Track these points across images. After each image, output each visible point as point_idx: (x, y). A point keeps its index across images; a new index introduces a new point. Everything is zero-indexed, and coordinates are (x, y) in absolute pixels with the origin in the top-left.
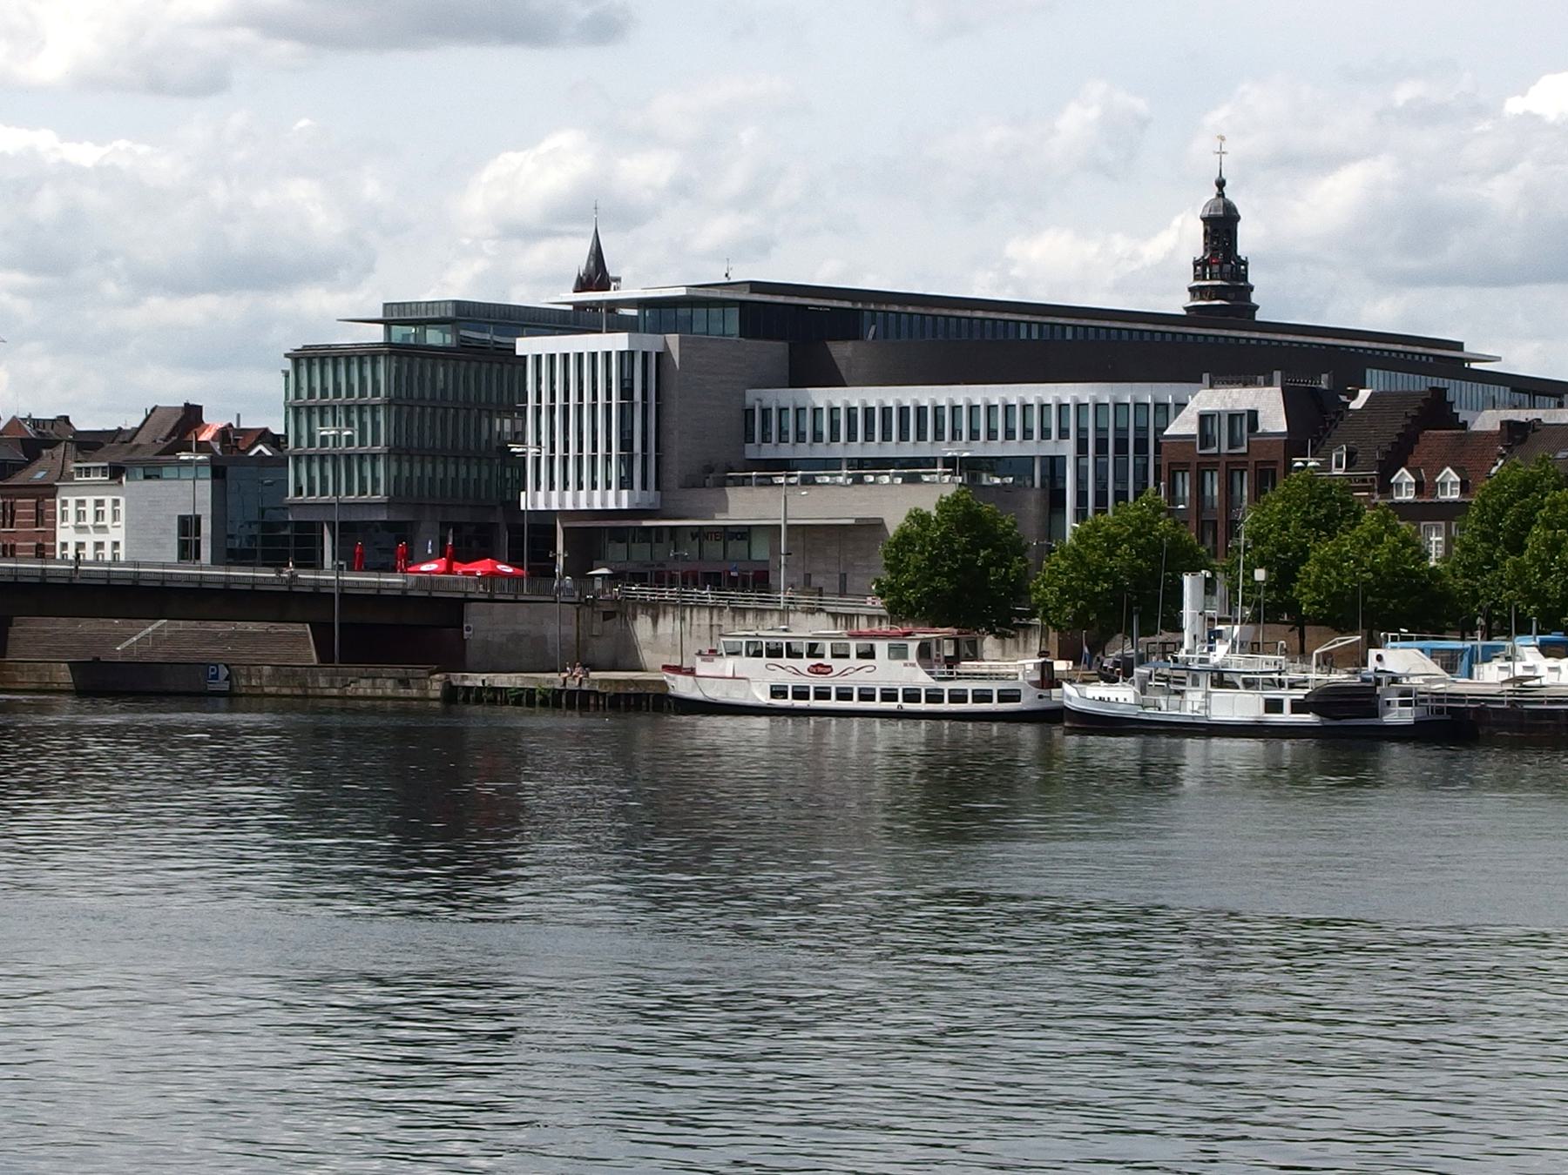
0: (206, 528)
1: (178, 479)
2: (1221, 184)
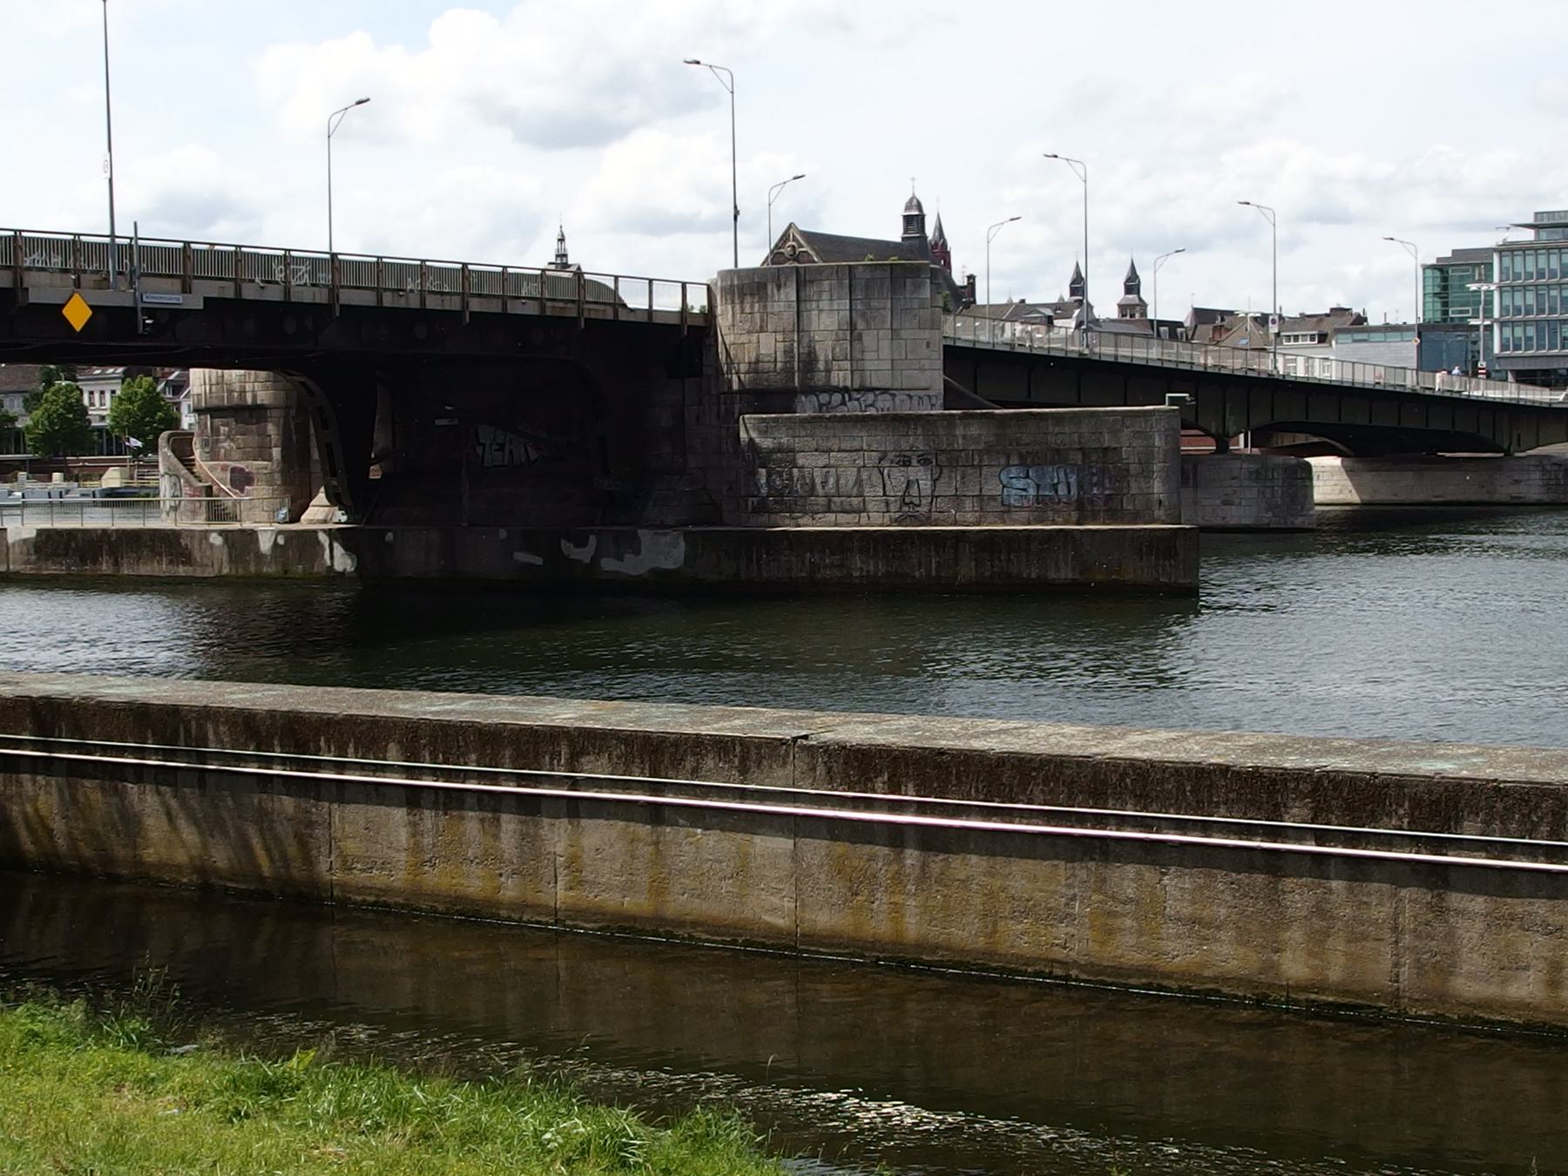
1: (1385, 341)
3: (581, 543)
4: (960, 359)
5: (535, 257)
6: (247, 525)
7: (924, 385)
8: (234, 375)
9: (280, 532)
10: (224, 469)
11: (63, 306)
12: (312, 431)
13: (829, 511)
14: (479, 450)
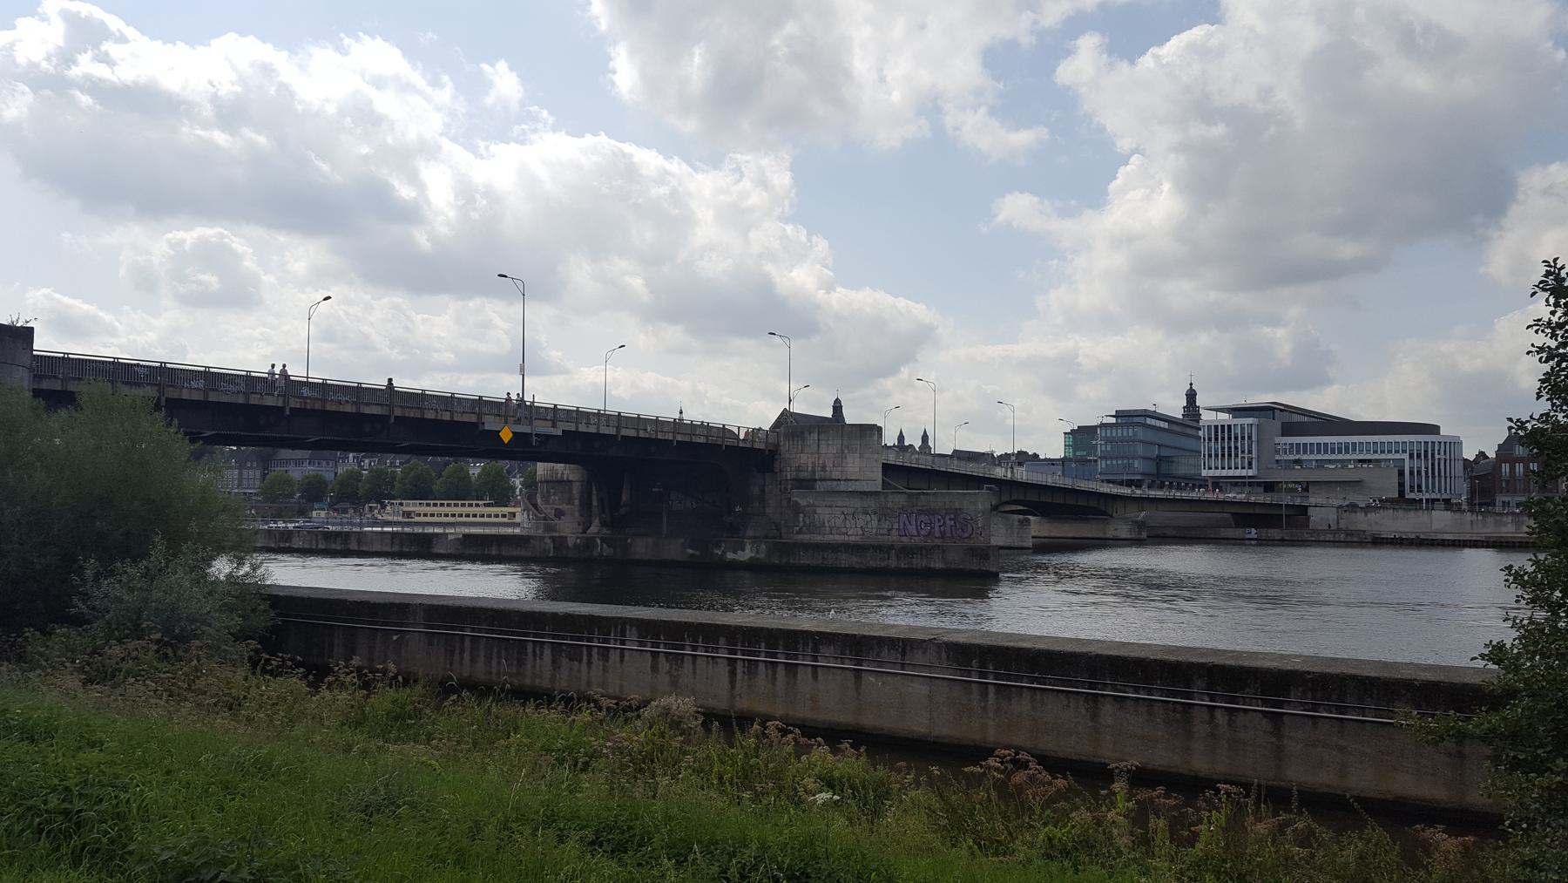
3: (718, 547)
4: (887, 468)
5: (377, 380)
6: (562, 534)
7: (874, 478)
8: (559, 467)
9: (578, 538)
10: (551, 508)
11: (499, 432)
12: (594, 492)
13: (831, 534)
14: (670, 502)
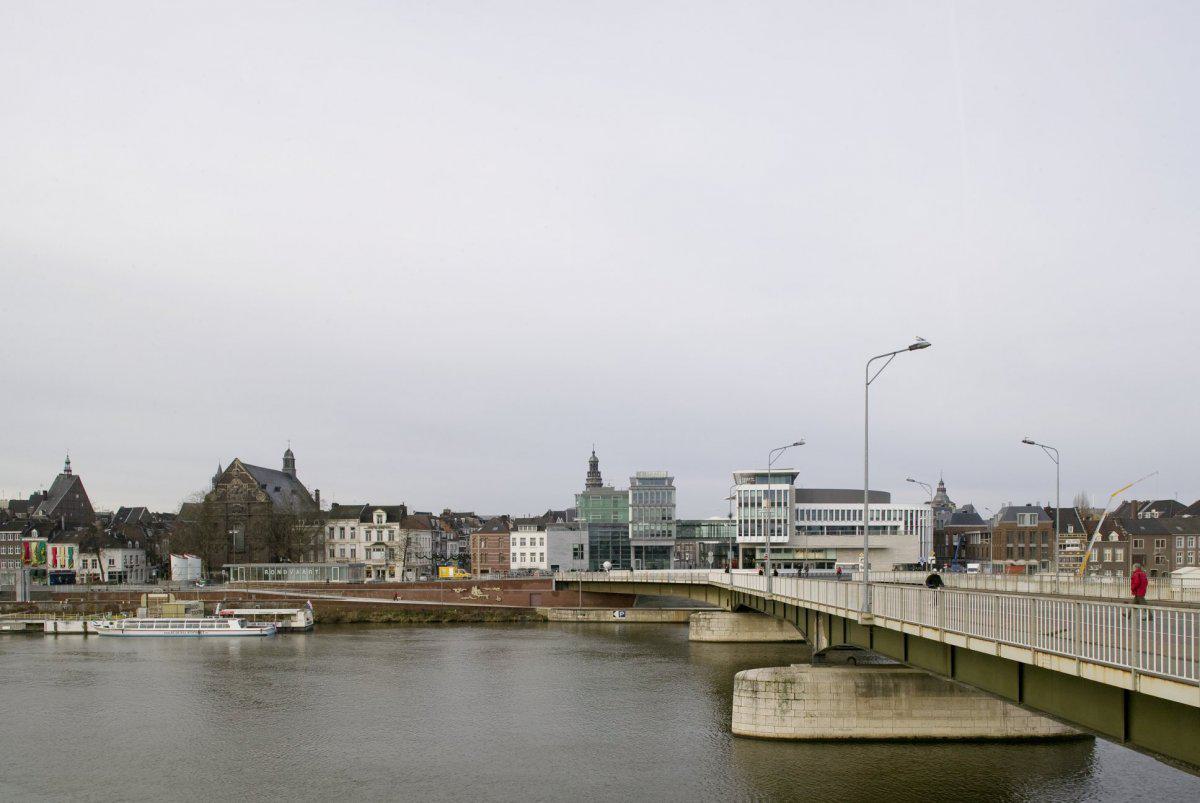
0: (586, 548)
2: (594, 453)
